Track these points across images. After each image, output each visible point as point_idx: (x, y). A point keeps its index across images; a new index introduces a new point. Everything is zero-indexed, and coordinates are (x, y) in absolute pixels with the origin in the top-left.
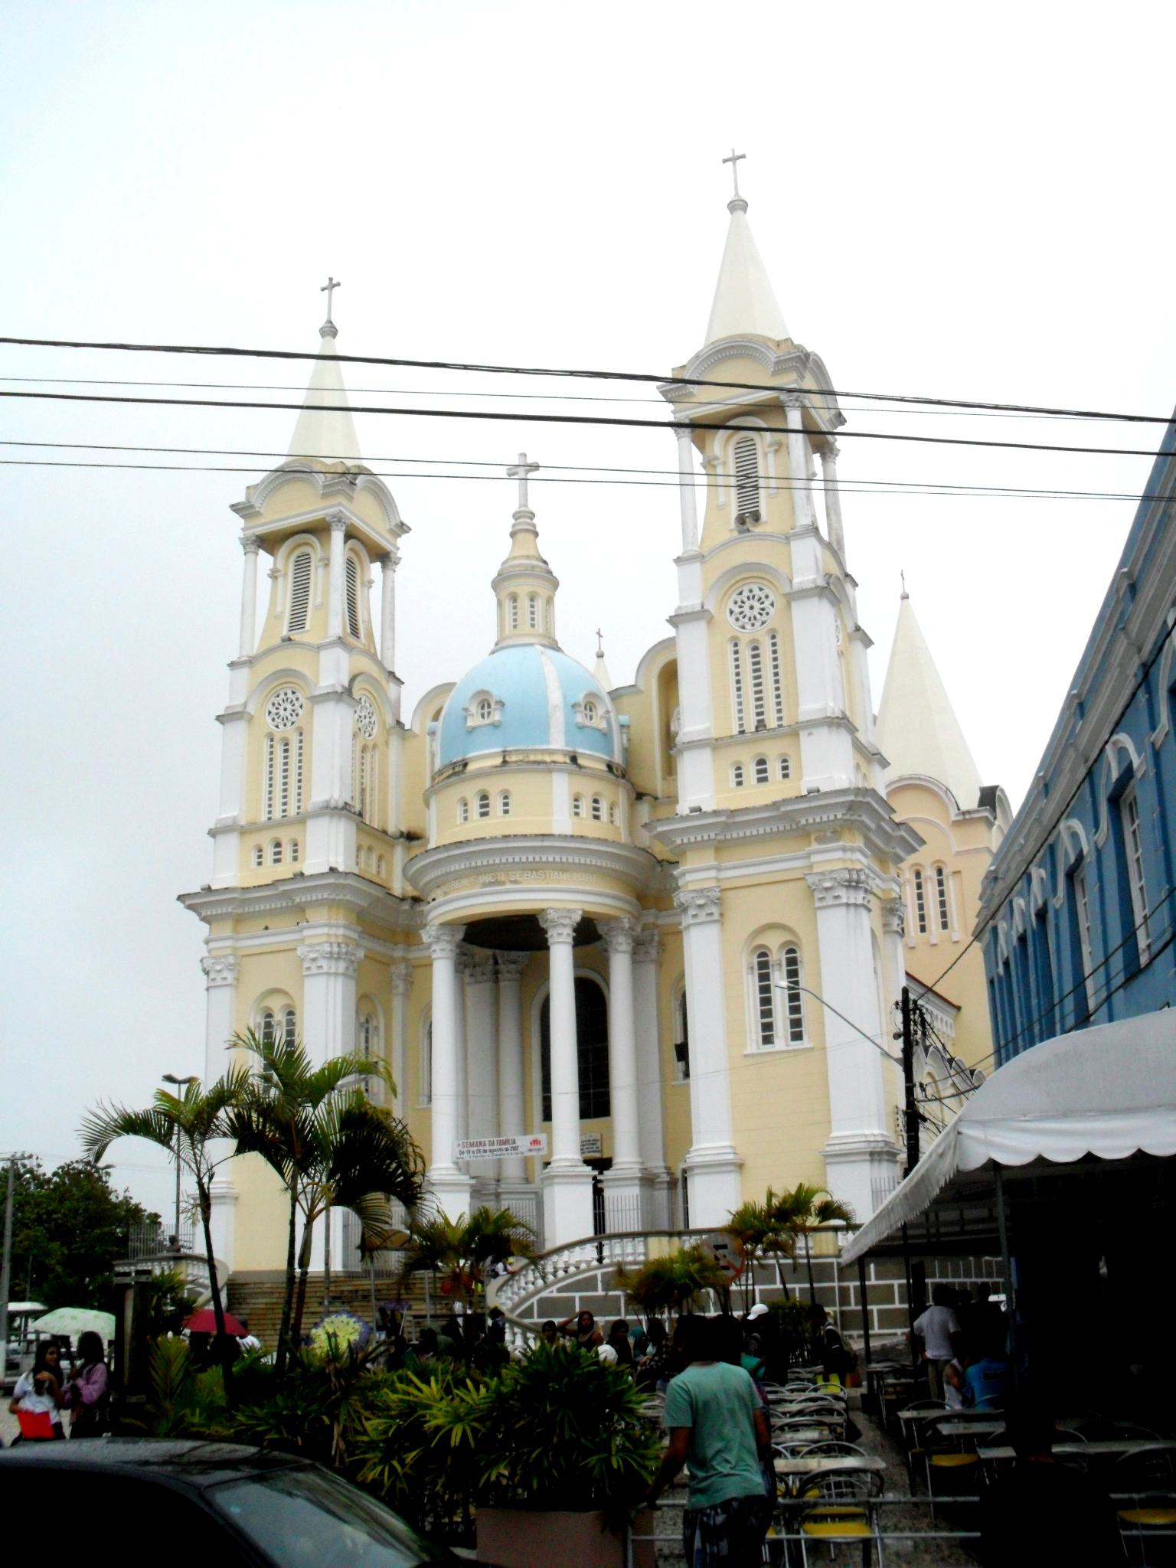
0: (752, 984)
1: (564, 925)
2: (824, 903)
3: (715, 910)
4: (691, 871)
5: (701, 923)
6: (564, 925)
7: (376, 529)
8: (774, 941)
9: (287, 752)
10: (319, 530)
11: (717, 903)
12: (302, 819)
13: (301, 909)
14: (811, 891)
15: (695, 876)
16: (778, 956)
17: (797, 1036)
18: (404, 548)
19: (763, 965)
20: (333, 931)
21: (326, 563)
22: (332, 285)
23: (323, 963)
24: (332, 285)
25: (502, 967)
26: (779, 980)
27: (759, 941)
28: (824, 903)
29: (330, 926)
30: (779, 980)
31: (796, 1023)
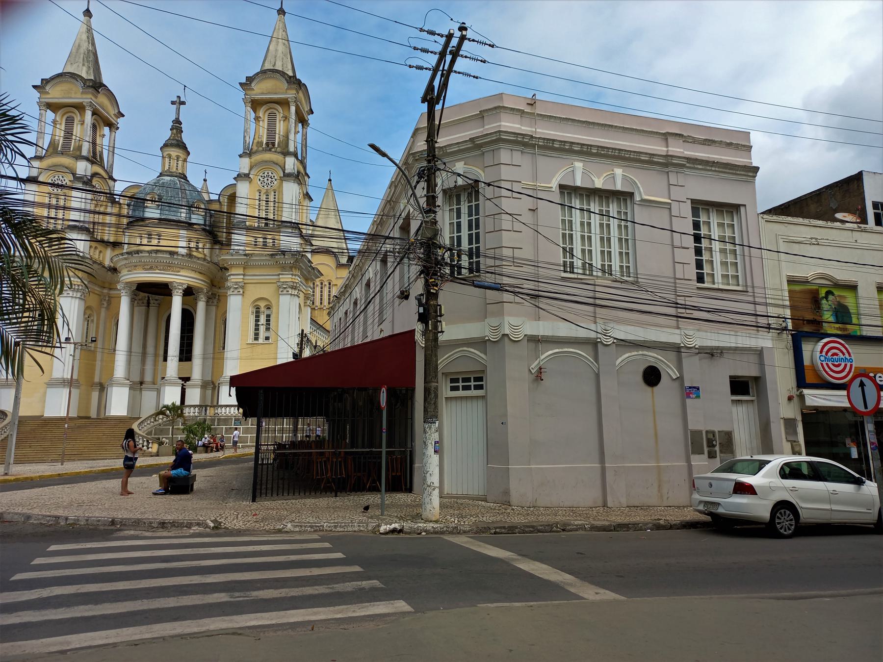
0: (252, 318)
7: (110, 112)
10: (284, 103)
11: (242, 287)
14: (279, 287)
15: (235, 277)
18: (311, 118)
25: (151, 302)
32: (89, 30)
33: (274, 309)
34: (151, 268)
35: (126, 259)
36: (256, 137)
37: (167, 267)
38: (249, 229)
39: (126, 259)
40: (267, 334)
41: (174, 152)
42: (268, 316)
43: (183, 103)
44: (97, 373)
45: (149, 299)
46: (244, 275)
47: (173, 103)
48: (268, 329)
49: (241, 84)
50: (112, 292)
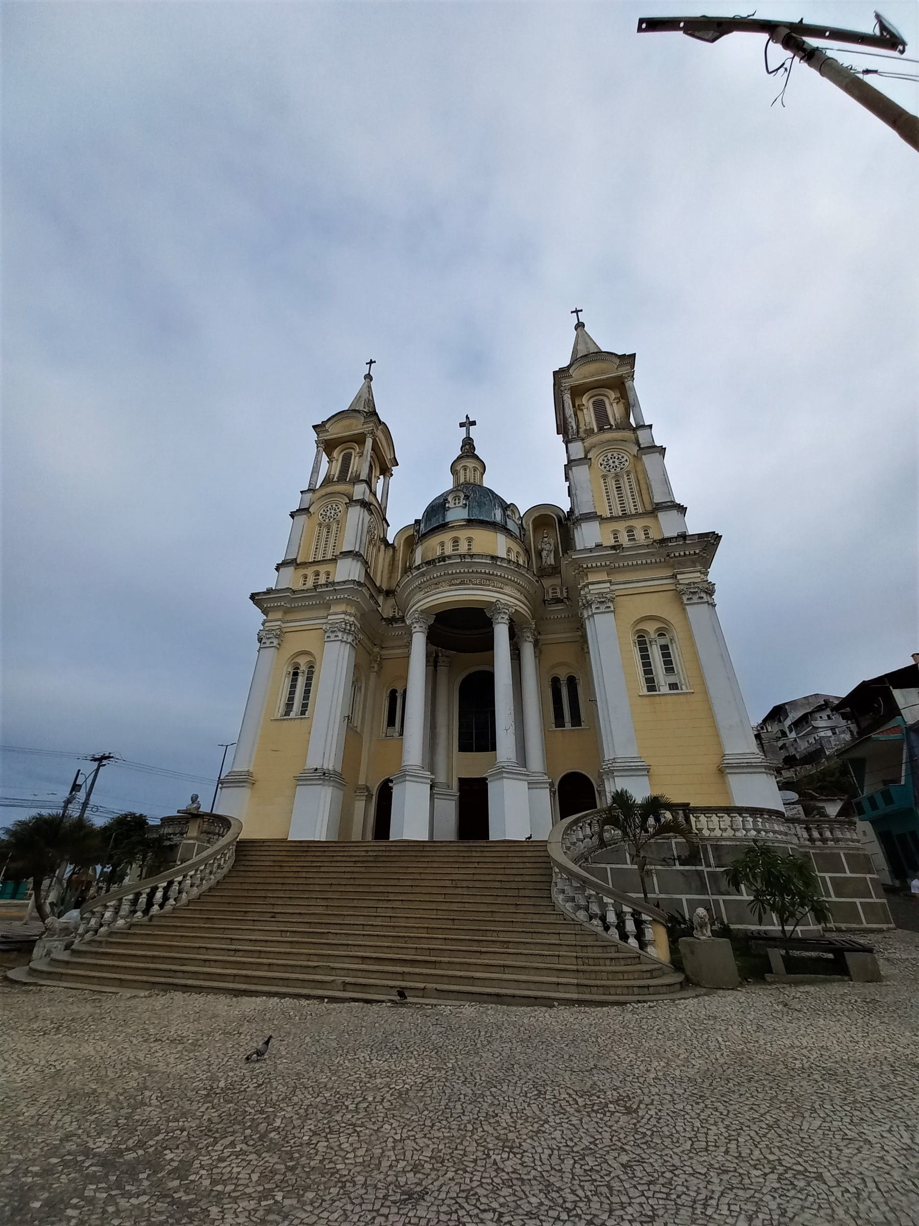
1: (505, 613)
2: (692, 602)
3: (276, 642)
4: (593, 583)
5: (603, 613)
6: (505, 613)
8: (303, 661)
9: (331, 526)
11: (607, 601)
12: (334, 560)
13: (328, 606)
15: (596, 584)
16: (303, 668)
17: (303, 713)
19: (296, 674)
20: (347, 617)
21: (361, 455)
22: (371, 362)
23: (340, 634)
24: (371, 362)
25: (440, 659)
26: (301, 681)
27: (640, 627)
28: (692, 602)
29: (345, 613)
30: (301, 681)
31: (305, 706)
32: (370, 387)
33: (678, 633)
34: (462, 583)
35: (423, 574)
36: (582, 425)
37: (487, 580)
38: (602, 519)
39: (423, 574)
40: (672, 679)
41: (471, 463)
42: (665, 648)
43: (474, 423)
44: (363, 768)
45: (437, 656)
46: (610, 582)
47: (462, 425)
48: (669, 668)
49: (314, 427)
50: (384, 652)
